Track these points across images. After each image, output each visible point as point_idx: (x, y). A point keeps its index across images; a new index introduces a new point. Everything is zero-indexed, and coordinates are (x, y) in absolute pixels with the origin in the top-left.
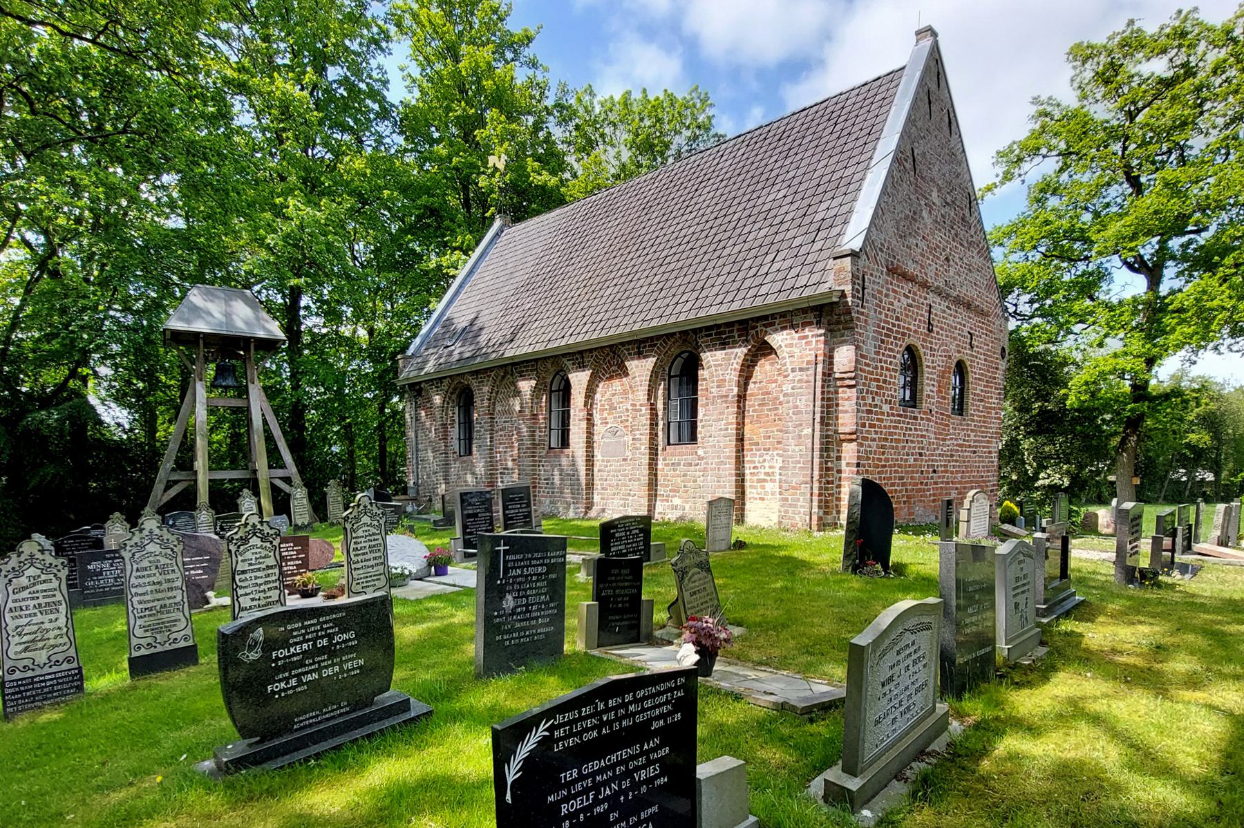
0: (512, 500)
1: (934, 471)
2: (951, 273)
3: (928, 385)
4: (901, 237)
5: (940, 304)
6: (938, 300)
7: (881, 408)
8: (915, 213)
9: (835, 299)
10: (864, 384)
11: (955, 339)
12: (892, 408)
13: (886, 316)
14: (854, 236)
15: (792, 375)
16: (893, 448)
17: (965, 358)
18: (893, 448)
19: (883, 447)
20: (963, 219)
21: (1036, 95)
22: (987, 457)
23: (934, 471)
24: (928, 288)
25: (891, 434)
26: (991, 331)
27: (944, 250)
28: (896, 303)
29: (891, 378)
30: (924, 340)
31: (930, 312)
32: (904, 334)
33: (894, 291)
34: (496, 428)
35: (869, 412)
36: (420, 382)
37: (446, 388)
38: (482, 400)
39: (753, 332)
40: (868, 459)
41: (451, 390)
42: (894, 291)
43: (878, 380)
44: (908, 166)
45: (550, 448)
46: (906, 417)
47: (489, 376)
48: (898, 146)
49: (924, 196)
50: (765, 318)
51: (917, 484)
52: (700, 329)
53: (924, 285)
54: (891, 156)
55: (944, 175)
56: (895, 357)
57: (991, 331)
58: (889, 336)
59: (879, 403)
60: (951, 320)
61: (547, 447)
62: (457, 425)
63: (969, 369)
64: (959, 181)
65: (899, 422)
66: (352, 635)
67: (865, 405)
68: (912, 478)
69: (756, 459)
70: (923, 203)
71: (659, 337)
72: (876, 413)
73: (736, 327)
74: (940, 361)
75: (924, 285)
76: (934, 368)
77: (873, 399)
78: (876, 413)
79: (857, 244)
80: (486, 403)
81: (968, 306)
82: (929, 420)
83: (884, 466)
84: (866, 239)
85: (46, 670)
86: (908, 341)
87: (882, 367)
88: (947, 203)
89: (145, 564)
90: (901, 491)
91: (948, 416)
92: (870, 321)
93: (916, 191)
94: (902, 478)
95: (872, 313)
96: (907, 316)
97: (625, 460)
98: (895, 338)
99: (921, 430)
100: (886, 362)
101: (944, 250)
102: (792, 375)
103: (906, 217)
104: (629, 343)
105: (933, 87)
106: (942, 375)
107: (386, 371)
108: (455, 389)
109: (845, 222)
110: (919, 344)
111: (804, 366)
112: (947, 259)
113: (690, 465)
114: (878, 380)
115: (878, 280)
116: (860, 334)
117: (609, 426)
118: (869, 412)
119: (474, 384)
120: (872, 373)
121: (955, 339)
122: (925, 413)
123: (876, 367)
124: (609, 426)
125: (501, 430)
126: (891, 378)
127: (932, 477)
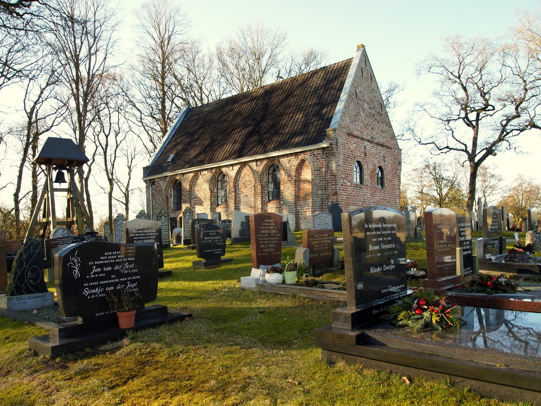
3: (366, 175)
4: (352, 122)
5: (369, 146)
6: (368, 143)
7: (347, 184)
8: (357, 113)
11: (377, 158)
12: (351, 184)
13: (347, 151)
16: (352, 198)
17: (382, 165)
18: (352, 198)
20: (378, 113)
22: (395, 204)
24: (364, 140)
25: (351, 193)
27: (370, 125)
28: (351, 146)
30: (363, 159)
32: (355, 157)
34: (192, 197)
36: (155, 179)
40: (342, 202)
41: (170, 181)
43: (345, 174)
44: (353, 96)
53: (362, 139)
58: (349, 158)
59: (346, 182)
62: (172, 197)
64: (376, 99)
67: (340, 182)
69: (303, 204)
72: (345, 186)
75: (362, 139)
76: (368, 169)
77: (343, 181)
78: (345, 186)
81: (382, 146)
82: (367, 189)
87: (346, 169)
88: (371, 108)
95: (342, 150)
96: (355, 150)
97: (251, 207)
99: (364, 192)
100: (348, 167)
103: (354, 116)
105: (363, 66)
108: (172, 181)
110: (361, 161)
111: (318, 169)
112: (372, 128)
114: (345, 174)
120: (342, 171)
121: (377, 158)
123: (344, 169)
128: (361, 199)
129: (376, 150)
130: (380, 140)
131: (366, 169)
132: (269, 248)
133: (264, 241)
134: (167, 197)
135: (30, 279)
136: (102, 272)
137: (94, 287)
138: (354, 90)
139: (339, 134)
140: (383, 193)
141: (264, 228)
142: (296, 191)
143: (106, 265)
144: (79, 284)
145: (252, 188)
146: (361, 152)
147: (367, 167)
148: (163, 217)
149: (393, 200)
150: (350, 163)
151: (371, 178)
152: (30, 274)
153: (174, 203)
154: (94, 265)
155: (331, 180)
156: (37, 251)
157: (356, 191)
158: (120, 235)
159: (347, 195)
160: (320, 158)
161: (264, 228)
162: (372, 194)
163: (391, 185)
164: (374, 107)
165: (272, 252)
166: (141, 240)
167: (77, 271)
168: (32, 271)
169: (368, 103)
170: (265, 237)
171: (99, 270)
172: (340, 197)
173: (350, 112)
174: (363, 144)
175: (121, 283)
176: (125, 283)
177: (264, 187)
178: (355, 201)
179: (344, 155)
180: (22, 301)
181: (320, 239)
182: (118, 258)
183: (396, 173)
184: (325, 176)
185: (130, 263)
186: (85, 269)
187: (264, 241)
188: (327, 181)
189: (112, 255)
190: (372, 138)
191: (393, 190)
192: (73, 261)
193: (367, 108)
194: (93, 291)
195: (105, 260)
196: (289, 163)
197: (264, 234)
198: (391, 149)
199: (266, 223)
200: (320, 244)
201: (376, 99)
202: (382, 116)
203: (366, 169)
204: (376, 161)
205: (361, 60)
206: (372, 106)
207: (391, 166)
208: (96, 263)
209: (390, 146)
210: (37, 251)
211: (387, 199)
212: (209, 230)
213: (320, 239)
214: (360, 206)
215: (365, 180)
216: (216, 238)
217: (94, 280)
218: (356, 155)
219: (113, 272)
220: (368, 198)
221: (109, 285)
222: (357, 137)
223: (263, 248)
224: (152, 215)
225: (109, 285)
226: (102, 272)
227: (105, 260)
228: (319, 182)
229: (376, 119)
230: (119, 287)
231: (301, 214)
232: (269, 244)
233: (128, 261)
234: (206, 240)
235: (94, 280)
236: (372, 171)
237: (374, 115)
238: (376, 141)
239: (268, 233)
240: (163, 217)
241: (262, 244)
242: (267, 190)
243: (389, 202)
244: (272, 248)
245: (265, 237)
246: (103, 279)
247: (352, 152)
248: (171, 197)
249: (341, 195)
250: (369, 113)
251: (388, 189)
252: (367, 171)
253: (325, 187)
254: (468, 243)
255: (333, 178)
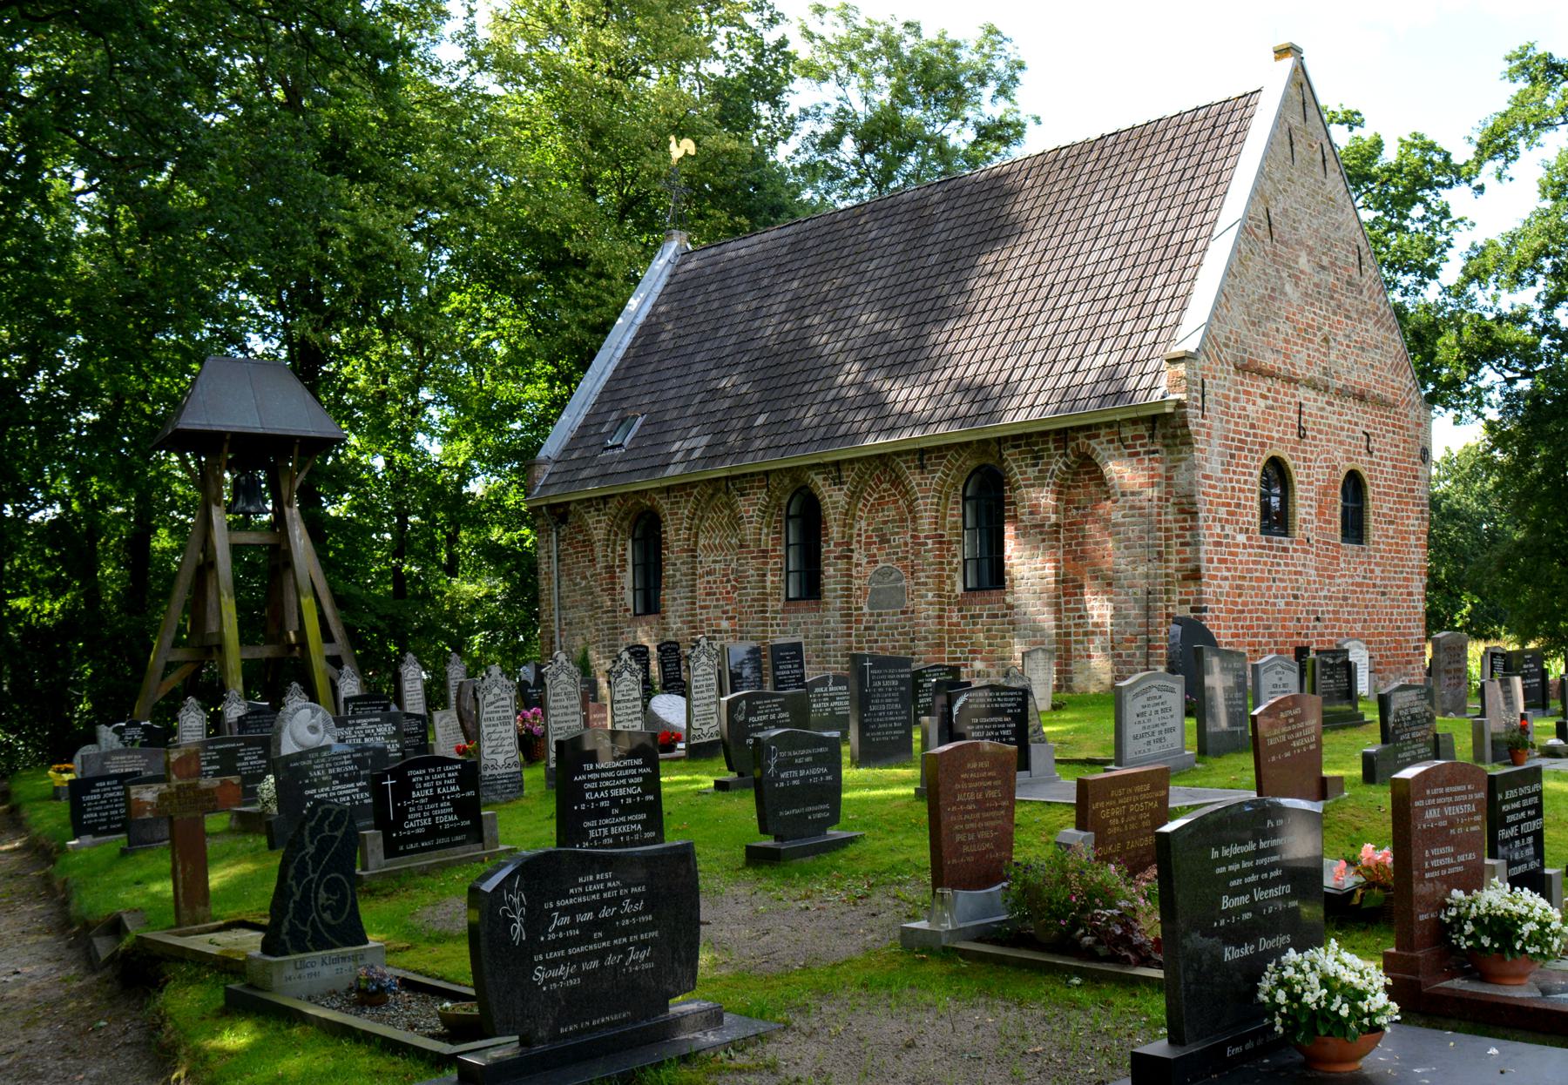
0: (783, 658)
1: (1318, 619)
2: (1333, 357)
3: (1303, 506)
4: (1254, 324)
5: (1315, 401)
6: (1312, 394)
7: (1234, 538)
8: (1273, 290)
9: (1168, 410)
10: (1209, 511)
11: (1341, 443)
12: (1249, 539)
13: (1237, 424)
14: (1189, 338)
15: (1122, 500)
16: (1253, 588)
17: (1359, 467)
18: (1253, 588)
19: (1239, 587)
20: (1348, 283)
21: (1515, 47)
22: (1404, 601)
23: (1318, 619)
24: (1296, 382)
25: (1249, 571)
26: (1401, 427)
27: (1320, 329)
28: (1250, 407)
29: (1246, 499)
30: (1293, 449)
31: (1300, 412)
32: (1263, 445)
33: (1246, 392)
34: (700, 571)
35: (1218, 544)
36: (568, 503)
37: (613, 511)
38: (678, 530)
39: (1073, 444)
40: (1218, 602)
41: (621, 514)
42: (1246, 392)
43: (1229, 505)
44: (1260, 233)
45: (788, 599)
46: (1271, 548)
47: (689, 495)
48: (1247, 210)
49: (1285, 265)
50: (1088, 427)
51: (1291, 635)
52: (1006, 439)
53: (1291, 380)
54: (1237, 227)
55: (1317, 231)
56: (1251, 474)
57: (1401, 427)
58: (1242, 449)
59: (1231, 533)
60: (1334, 420)
61: (783, 598)
62: (630, 568)
63: (1367, 481)
64: (1341, 234)
65: (1261, 555)
66: (786, 715)
67: (1212, 535)
68: (1283, 627)
70: (1285, 275)
71: (948, 447)
72: (1228, 545)
73: (1051, 438)
74: (1320, 475)
75: (1291, 380)
76: (1310, 483)
77: (1223, 528)
78: (1228, 545)
79: (1192, 345)
80: (683, 534)
81: (1361, 397)
82: (1306, 552)
83: (1242, 612)
84: (1205, 335)
85: (504, 771)
86: (1269, 453)
87: (1233, 489)
88: (1323, 268)
89: (558, 690)
90: (1268, 644)
91: (1337, 546)
92: (1214, 433)
93: (1274, 262)
94: (1269, 627)
95: (1217, 424)
96: (1266, 421)
97: (903, 613)
98: (1250, 451)
99: (1294, 565)
100: (1238, 481)
101: (1320, 329)
102: (1122, 500)
103: (1261, 300)
104: (908, 452)
105: (1296, 120)
106: (1324, 492)
107: (1470, 633)
108: (627, 514)
109: (1183, 309)
110: (1285, 455)
112: (1326, 340)
113: (996, 616)
114: (1229, 505)
115: (1222, 383)
116: (1201, 451)
117: (880, 565)
118: (1218, 544)
119: (664, 506)
120: (1219, 496)
121: (1341, 443)
122: (1299, 543)
123: (1225, 489)
124: (880, 565)
125: (709, 573)
126: (1246, 499)
127: (1315, 627)
128: (1285, 589)
129: (1340, 414)
130: (1354, 377)
131: (1301, 482)
132: (977, 841)
133: (964, 822)
134: (610, 569)
135: (325, 909)
136: (572, 926)
137: (554, 964)
138: (1261, 209)
139: (1209, 369)
140: (1362, 563)
141: (964, 786)
142: (1057, 561)
143: (583, 908)
144: (523, 956)
145: (906, 544)
146: (1286, 425)
147: (1308, 476)
148: (626, 675)
149: (1399, 587)
150: (1247, 466)
151: (1320, 513)
152: (322, 894)
153: (635, 589)
154: (555, 909)
155: (1182, 528)
156: (339, 834)
157: (1265, 564)
158: (494, 736)
159: (1234, 578)
160: (1142, 450)
161: (964, 786)
162: (1325, 569)
163: (1391, 533)
164: (1332, 264)
165: (988, 851)
166: (604, 789)
167: (519, 926)
168: (327, 890)
169: (1311, 251)
170: (969, 812)
171: (566, 920)
172: (1209, 585)
173: (1249, 288)
174: (1293, 396)
175: (613, 950)
176: (623, 949)
177: (950, 542)
178: (1263, 596)
179: (1226, 438)
180: (307, 971)
181: (1127, 800)
182: (607, 889)
183: (1412, 491)
184: (1159, 514)
185: (635, 899)
186: (537, 920)
187: (964, 822)
188: (1167, 530)
189: (595, 882)
190: (1326, 372)
191: (1398, 552)
192: (510, 902)
193: (1308, 269)
194: (554, 974)
195: (578, 895)
196: (1036, 465)
197: (966, 803)
198: (1394, 406)
199: (969, 771)
200: (1127, 814)
201: (1341, 234)
202: (1361, 292)
203: (1301, 482)
204: (1339, 454)
205: (1286, 100)
206: (1325, 261)
207: (1394, 467)
208: (559, 904)
209: (1391, 397)
210: (339, 834)
211: (1378, 582)
212: (793, 749)
213: (1127, 800)
214: (1279, 612)
215: (1298, 522)
216: (813, 772)
217: (555, 945)
218: (1269, 438)
219: (596, 924)
220: (1309, 582)
221: (587, 956)
222: (1271, 375)
223: (961, 843)
224: (561, 630)
225: (587, 956)
226: (572, 926)
227: (578, 895)
228: (1137, 533)
229: (1339, 307)
230: (610, 960)
231: (1076, 642)
232: (979, 830)
233: (630, 895)
234: (785, 780)
235: (555, 945)
236: (1326, 488)
237: (1333, 290)
238: (1340, 384)
239: (976, 801)
240: (626, 675)
241: (959, 832)
242: (959, 554)
243: (1384, 594)
244: (987, 840)
245: (969, 812)
246: (576, 942)
247: (1253, 426)
248: (623, 568)
249: (1214, 577)
250: (1316, 285)
251: (1382, 547)
252: (1307, 491)
253: (1159, 553)
254: (1530, 840)
255: (1185, 520)
